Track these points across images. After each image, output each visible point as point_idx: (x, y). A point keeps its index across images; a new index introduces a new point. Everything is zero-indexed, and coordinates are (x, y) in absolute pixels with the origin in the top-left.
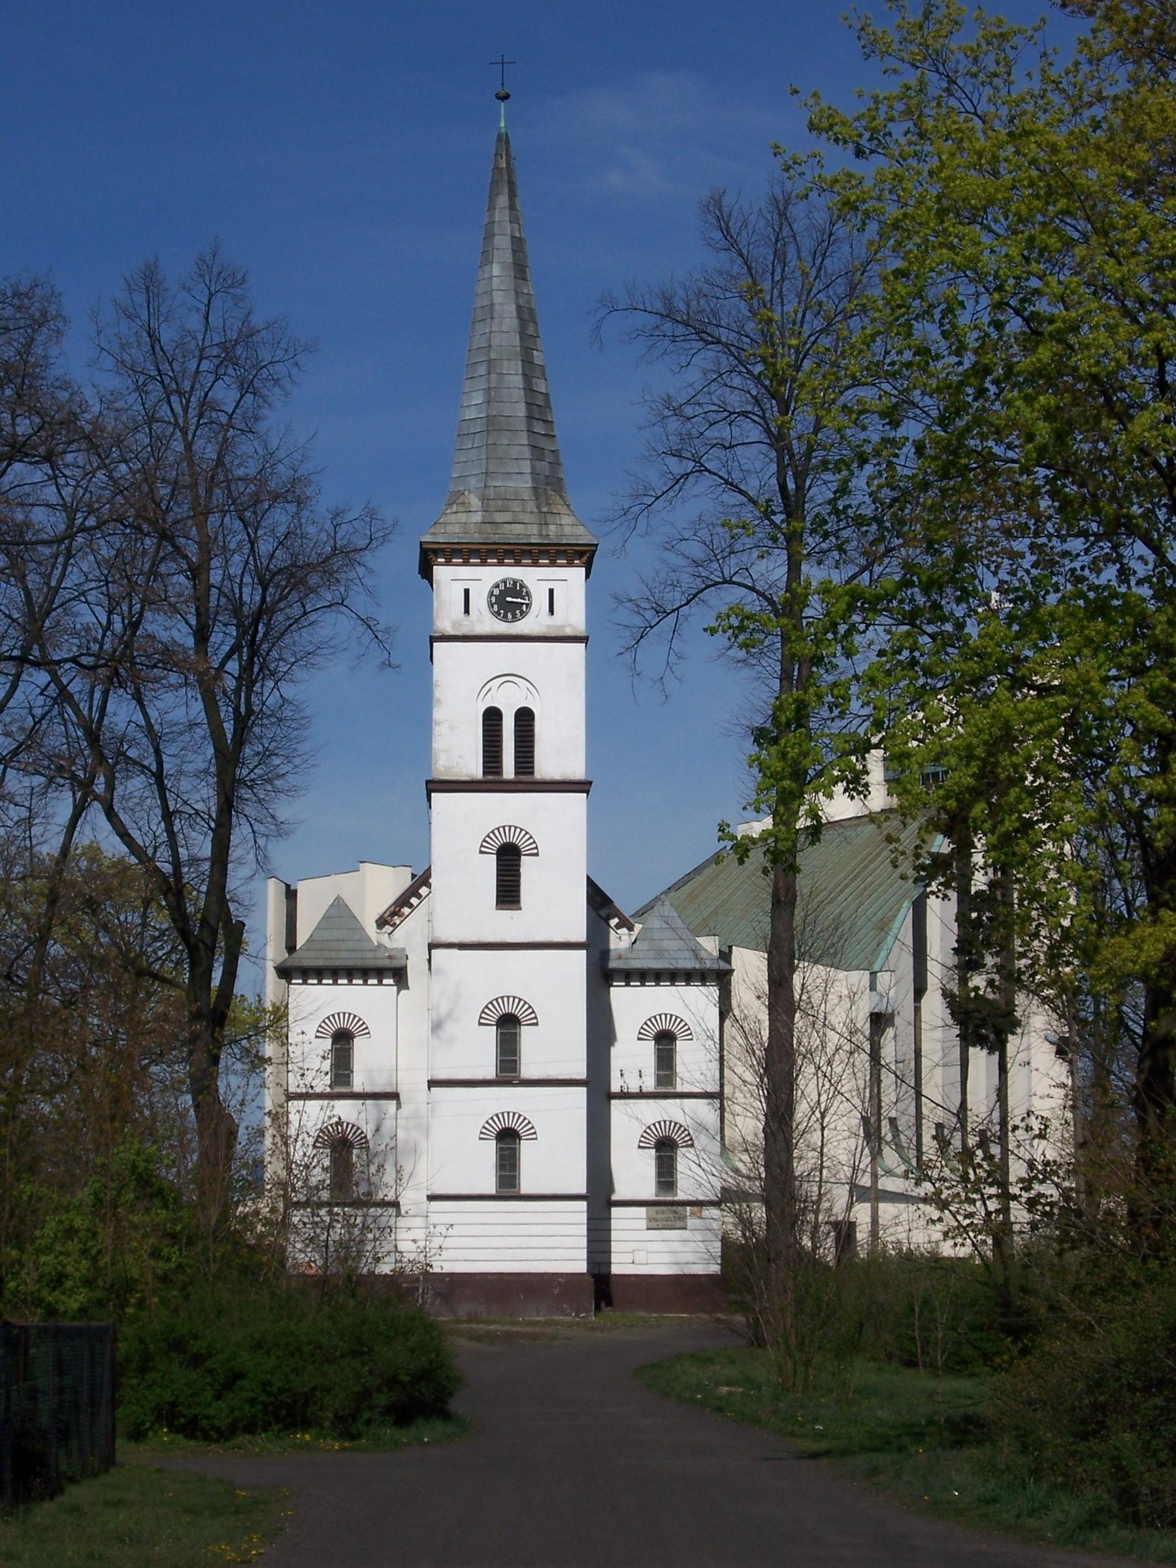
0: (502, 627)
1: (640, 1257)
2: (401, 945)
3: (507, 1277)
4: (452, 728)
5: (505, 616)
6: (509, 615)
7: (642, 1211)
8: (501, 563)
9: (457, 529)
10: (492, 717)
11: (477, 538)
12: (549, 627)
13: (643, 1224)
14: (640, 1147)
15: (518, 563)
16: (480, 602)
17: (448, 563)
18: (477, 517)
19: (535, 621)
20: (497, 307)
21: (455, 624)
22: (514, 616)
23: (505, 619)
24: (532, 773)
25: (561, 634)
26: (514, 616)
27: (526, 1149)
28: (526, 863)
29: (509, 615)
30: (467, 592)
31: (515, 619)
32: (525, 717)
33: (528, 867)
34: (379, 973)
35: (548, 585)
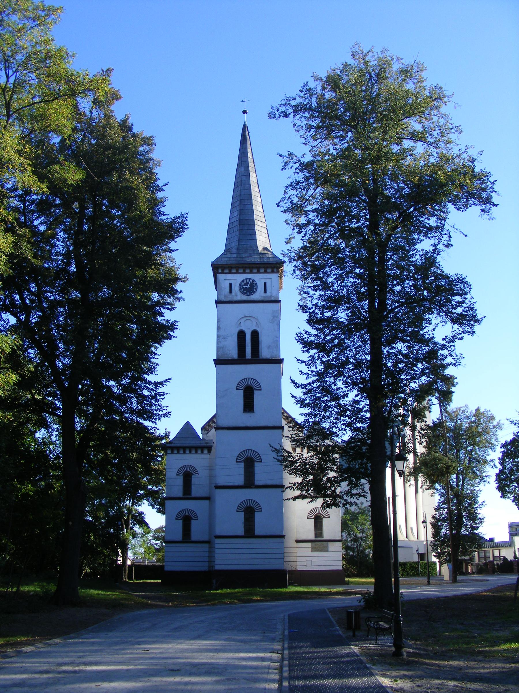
0: (244, 298)
1: (309, 564)
2: (211, 438)
3: (238, 176)
4: (224, 338)
5: (246, 293)
6: (248, 293)
7: (309, 545)
8: (244, 272)
9: (226, 259)
10: (241, 334)
11: (234, 262)
12: (264, 297)
13: (310, 549)
14: (308, 518)
15: (251, 272)
16: (236, 288)
17: (223, 272)
18: (235, 255)
19: (259, 295)
20: (243, 181)
21: (225, 296)
22: (250, 293)
23: (246, 294)
24: (259, 357)
25: (270, 300)
26: (250, 293)
27: (258, 516)
28: (256, 393)
29: (248, 293)
30: (231, 284)
31: (250, 294)
32: (255, 334)
33: (257, 396)
34: (202, 448)
35: (263, 282)
